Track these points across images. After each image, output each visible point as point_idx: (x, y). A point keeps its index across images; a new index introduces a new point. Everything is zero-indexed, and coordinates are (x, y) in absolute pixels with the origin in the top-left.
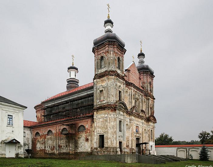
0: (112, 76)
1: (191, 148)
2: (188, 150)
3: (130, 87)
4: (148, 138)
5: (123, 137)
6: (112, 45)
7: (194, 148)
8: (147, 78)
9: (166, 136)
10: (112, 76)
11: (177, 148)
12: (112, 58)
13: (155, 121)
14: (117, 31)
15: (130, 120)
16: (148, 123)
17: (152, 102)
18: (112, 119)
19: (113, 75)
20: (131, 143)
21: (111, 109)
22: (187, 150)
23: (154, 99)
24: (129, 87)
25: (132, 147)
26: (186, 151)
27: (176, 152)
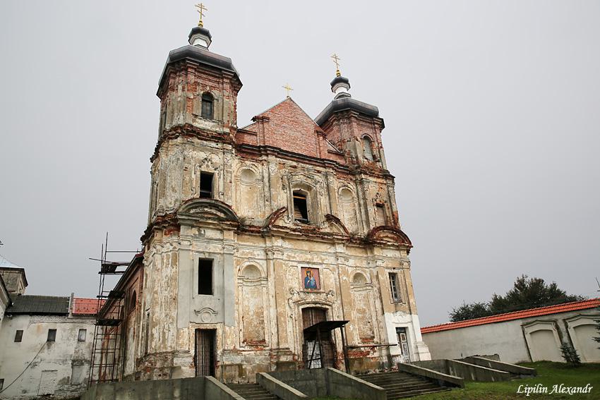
0: (175, 140)
1: (530, 320)
2: (562, 327)
3: (264, 158)
4: (378, 302)
5: (220, 313)
6: (182, 70)
7: (539, 319)
8: (351, 127)
9: (538, 283)
10: (176, 138)
11: (520, 322)
12: (179, 99)
13: (403, 242)
14: (359, 94)
15: (266, 251)
16: (372, 252)
17: (384, 187)
18: (168, 259)
19: (178, 137)
20: (274, 330)
21: (165, 227)
22: (557, 328)
23: (387, 176)
24: (260, 158)
25: (278, 344)
26: (555, 333)
27: (523, 340)
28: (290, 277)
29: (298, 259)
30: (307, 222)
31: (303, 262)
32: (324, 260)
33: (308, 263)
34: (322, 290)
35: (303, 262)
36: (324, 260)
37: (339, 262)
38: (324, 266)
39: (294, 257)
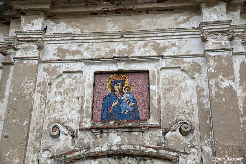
28: (59, 98)
29: (87, 55)
30: (160, 69)
31: (99, 60)
32: (165, 48)
33: (115, 60)
34: (151, 122)
35: (99, 60)
36: (165, 48)
37: (210, 45)
38: (163, 63)
39: (75, 53)
